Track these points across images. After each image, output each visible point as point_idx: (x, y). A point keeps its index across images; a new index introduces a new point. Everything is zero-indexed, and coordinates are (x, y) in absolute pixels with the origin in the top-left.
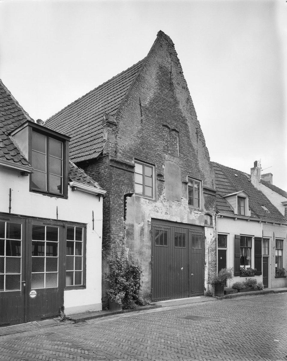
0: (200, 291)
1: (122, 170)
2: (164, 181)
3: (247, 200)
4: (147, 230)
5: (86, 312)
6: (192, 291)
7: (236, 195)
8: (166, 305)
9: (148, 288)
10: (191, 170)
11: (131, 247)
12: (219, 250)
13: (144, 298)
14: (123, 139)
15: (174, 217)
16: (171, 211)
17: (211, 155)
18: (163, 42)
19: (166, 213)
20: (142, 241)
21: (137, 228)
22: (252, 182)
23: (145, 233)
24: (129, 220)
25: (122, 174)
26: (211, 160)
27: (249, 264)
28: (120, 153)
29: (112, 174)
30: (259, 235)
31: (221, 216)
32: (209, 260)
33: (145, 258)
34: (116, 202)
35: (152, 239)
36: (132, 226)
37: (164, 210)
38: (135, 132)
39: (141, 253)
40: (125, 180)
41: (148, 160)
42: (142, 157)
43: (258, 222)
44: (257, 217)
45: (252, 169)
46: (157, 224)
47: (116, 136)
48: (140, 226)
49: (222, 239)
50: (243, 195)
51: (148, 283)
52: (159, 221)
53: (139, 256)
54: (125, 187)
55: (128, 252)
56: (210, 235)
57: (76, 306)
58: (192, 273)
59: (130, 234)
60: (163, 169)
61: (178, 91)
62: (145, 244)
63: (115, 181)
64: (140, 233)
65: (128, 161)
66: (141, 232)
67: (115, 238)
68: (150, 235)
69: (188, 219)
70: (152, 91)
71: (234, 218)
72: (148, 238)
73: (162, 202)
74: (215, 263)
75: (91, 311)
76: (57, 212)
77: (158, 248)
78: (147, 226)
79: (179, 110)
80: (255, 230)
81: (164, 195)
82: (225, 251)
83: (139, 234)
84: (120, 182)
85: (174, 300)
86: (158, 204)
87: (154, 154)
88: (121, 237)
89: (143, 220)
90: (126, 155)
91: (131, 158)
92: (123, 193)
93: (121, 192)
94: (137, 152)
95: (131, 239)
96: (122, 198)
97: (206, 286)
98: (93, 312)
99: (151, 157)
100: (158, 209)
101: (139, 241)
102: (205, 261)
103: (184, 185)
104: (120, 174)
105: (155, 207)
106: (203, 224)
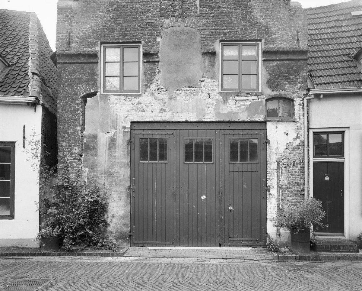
0: (257, 237)
1: (77, 65)
2: (158, 62)
4: (121, 140)
5: (13, 247)
6: (232, 236)
8: (135, 255)
9: (124, 225)
10: (227, 29)
11: (92, 167)
12: (314, 163)
13: (117, 239)
14: (81, 23)
15: (181, 115)
16: (174, 106)
19: (162, 110)
20: (111, 156)
21: (103, 139)
23: (117, 145)
24: (89, 130)
25: (78, 69)
28: (76, 42)
29: (61, 73)
32: (281, 183)
33: (117, 181)
34: (67, 108)
35: (131, 153)
36: (95, 137)
37: (158, 106)
38: (104, 6)
39: (109, 175)
40: (82, 76)
41: (127, 37)
42: (114, 36)
47: (71, 21)
48: (108, 135)
51: (124, 217)
52: (150, 125)
53: (107, 179)
54: (82, 86)
55: (86, 174)
56: (281, 137)
57: (7, 238)
58: (230, 205)
59: (89, 147)
60: (159, 43)
62: (117, 160)
63: (65, 82)
64: (109, 146)
65: (89, 49)
66: (110, 144)
67: (66, 156)
68: (128, 147)
69: (218, 114)
72: (124, 152)
73: (153, 94)
74: (302, 187)
75: (20, 246)
76: (24, 132)
77: (146, 165)
78: (122, 135)
81: (159, 82)
82: (342, 163)
83: (107, 147)
84: (74, 81)
85: (172, 248)
86: (146, 99)
87: (140, 26)
88: (75, 153)
89: (114, 127)
90: (87, 41)
91: (95, 44)
92: (80, 94)
93: (75, 94)
94: (106, 32)
95: (92, 156)
96: (79, 101)
97: (271, 229)
98: (23, 248)
99: (132, 32)
100: (144, 107)
101: (107, 157)
102: (268, 185)
103: (207, 58)
104: (74, 70)
105: (139, 104)
106: (260, 118)
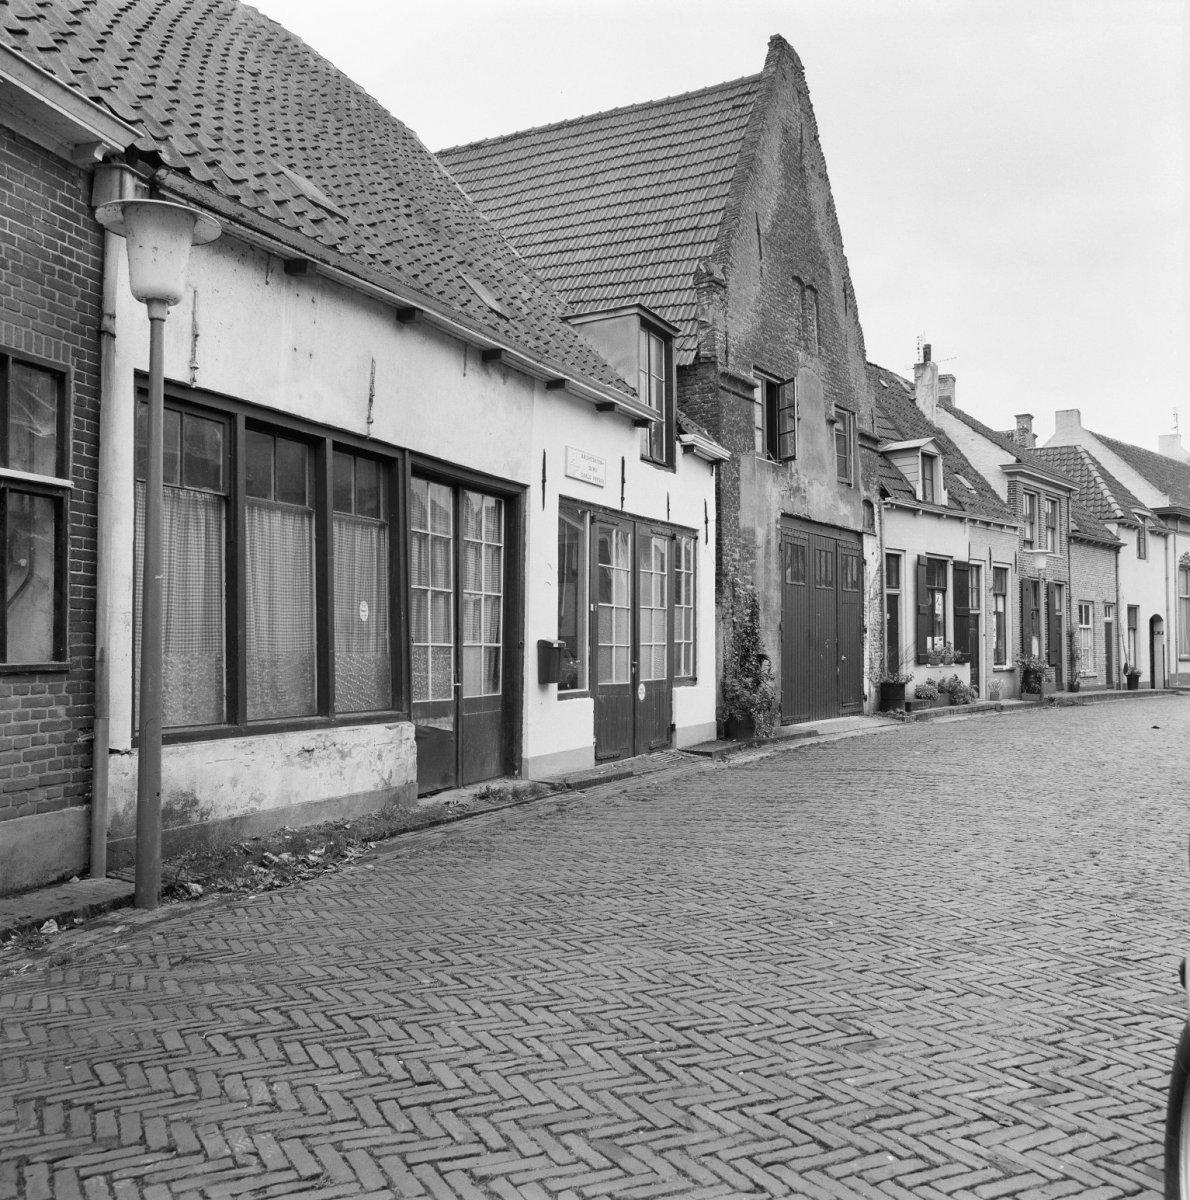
3: (940, 461)
7: (917, 449)
17: (868, 346)
18: (778, 44)
22: (920, 403)
26: (869, 359)
27: (12, 452)
30: (962, 556)
31: (892, 505)
43: (961, 519)
44: (957, 512)
45: (918, 367)
46: (801, 532)
49: (893, 560)
50: (932, 449)
56: (872, 552)
61: (814, 183)
65: (744, 374)
70: (776, 192)
71: (914, 512)
79: (816, 232)
80: (953, 542)
106: (859, 528)
